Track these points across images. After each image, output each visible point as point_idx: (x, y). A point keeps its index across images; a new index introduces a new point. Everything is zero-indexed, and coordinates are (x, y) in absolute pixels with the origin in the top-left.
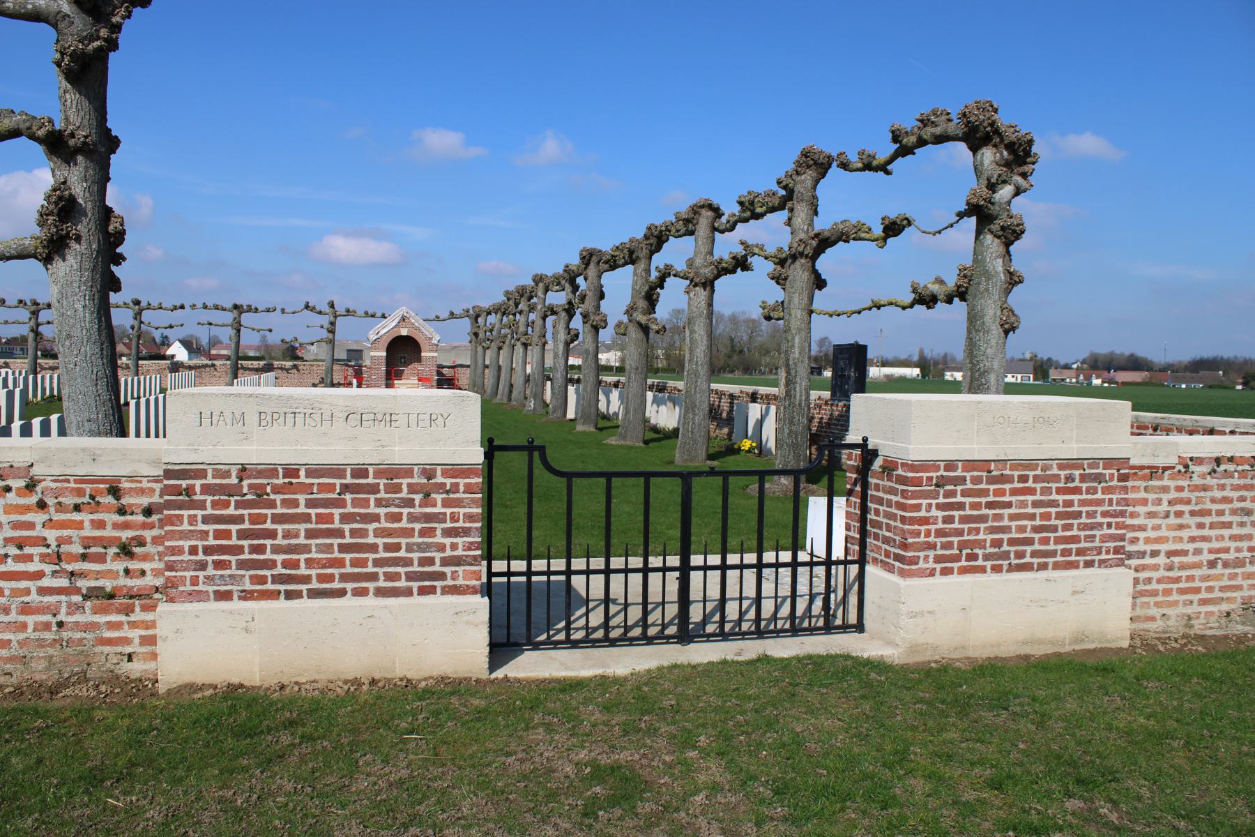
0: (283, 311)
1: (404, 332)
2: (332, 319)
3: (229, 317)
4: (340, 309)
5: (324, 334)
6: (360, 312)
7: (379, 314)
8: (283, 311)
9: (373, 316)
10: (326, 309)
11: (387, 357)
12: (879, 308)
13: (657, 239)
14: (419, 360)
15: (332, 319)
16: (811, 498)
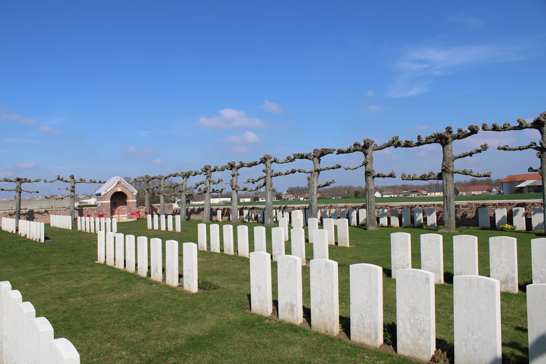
0: (45, 181)
1: (119, 190)
2: (73, 184)
3: (14, 185)
4: (77, 179)
5: (69, 193)
6: (88, 180)
7: (98, 181)
8: (45, 181)
9: (95, 182)
10: (69, 179)
11: (111, 203)
12: (288, 158)
13: (323, 153)
14: (125, 204)
15: (73, 184)
16: (392, 234)
